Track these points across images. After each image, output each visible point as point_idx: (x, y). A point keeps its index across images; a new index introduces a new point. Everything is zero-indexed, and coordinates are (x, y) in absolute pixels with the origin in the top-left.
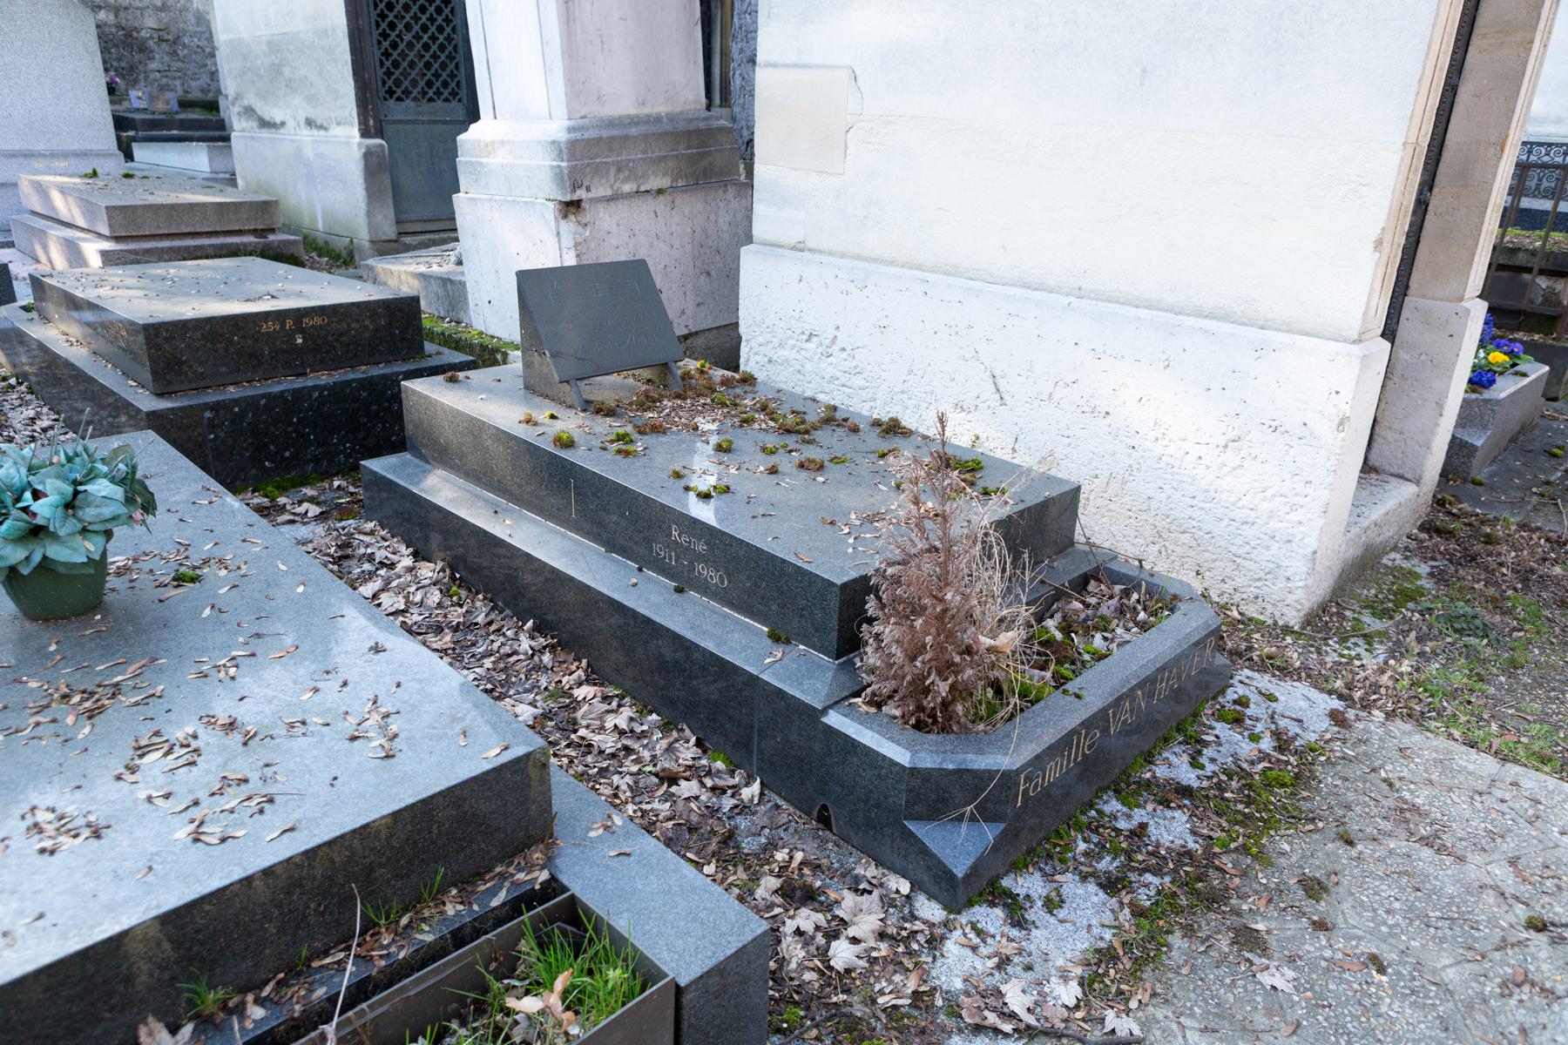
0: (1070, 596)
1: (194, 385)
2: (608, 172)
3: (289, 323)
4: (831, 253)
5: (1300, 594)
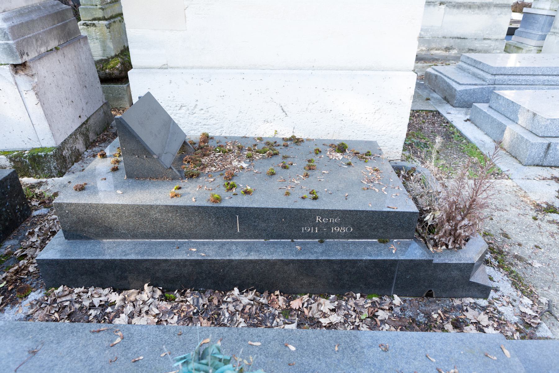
2: (32, 42)
4: (184, 68)
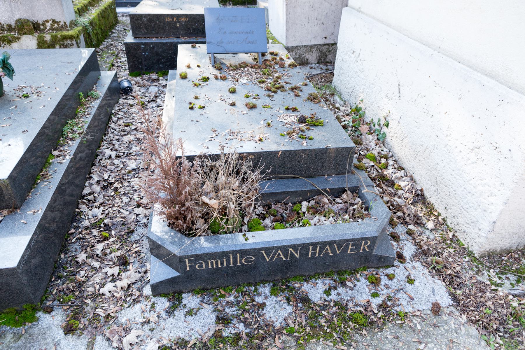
0: (323, 194)
1: (144, 36)
3: (175, 19)
5: (482, 240)
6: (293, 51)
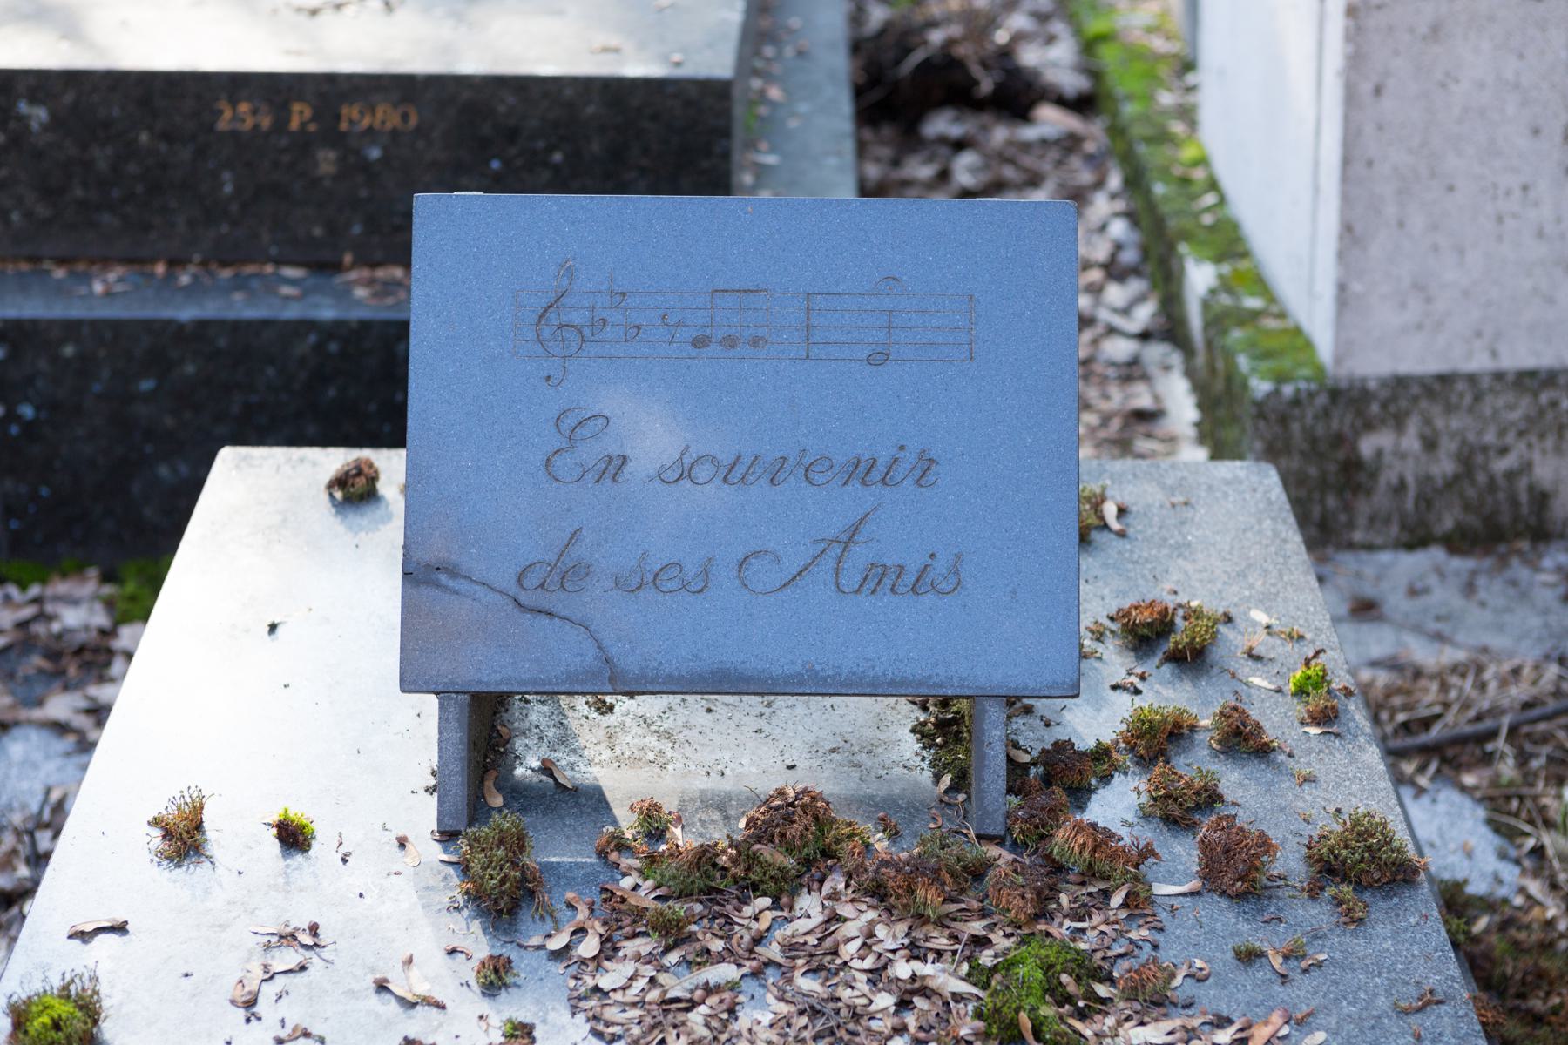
3: (300, 114)
6: (1399, 423)
